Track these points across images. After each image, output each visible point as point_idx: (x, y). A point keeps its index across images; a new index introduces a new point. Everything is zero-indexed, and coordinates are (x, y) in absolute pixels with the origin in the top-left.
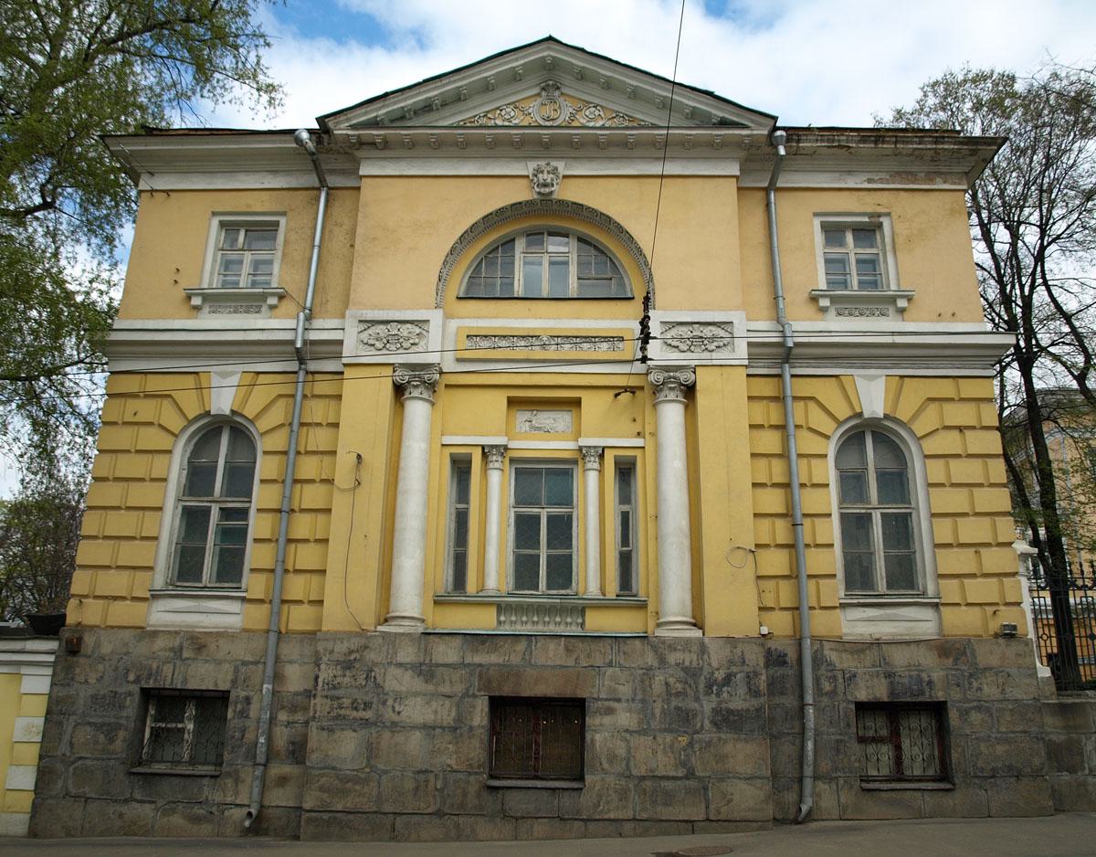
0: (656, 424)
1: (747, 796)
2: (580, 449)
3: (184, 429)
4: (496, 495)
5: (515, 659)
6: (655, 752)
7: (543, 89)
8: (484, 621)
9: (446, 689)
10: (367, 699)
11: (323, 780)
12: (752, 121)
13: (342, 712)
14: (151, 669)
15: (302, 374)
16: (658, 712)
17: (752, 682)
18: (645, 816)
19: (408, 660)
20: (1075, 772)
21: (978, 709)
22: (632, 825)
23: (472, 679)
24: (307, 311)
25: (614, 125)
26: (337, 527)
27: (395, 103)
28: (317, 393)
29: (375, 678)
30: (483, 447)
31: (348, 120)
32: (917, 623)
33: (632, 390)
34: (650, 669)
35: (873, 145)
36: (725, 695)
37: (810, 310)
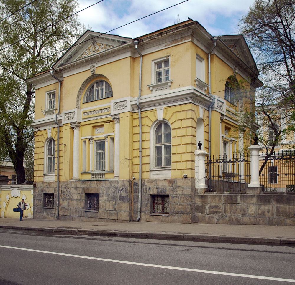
1: (125, 215)
3: (153, 124)
5: (88, 186)
10: (68, 194)
12: (128, 40)
13: (65, 197)
16: (110, 196)
18: (108, 218)
20: (203, 213)
21: (176, 196)
22: (106, 220)
27: (64, 58)
28: (134, 118)
30: (88, 139)
31: (57, 66)
32: (167, 175)
35: (161, 36)
36: (121, 193)
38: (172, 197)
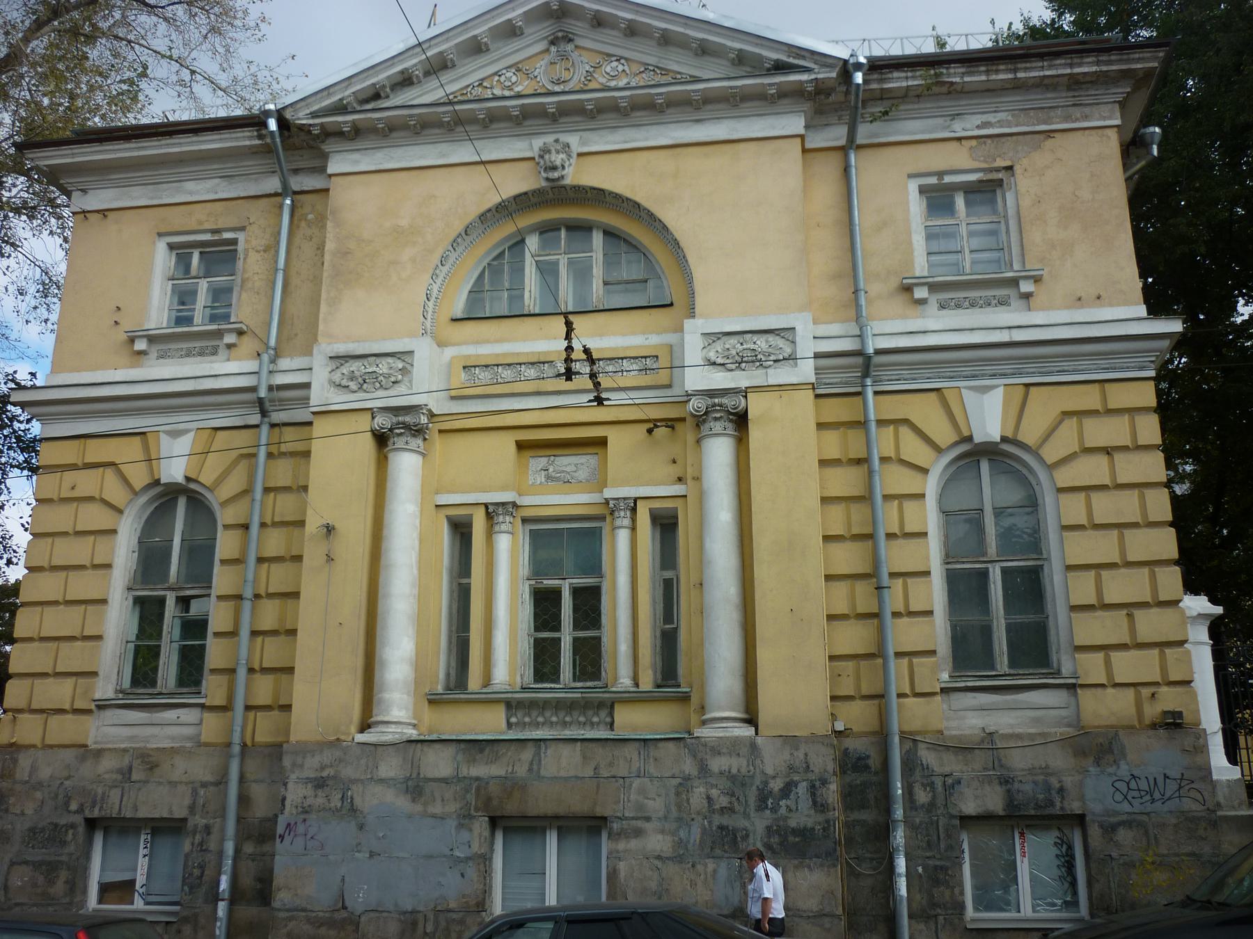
0: (699, 466)
2: (607, 501)
4: (507, 564)
5: (521, 771)
6: (693, 884)
7: (552, 43)
8: (489, 723)
9: (437, 809)
11: (291, 925)
14: (96, 795)
15: (265, 429)
17: (818, 793)
19: (392, 774)
23: (468, 796)
24: (272, 352)
25: (642, 84)
26: (308, 615)
29: (352, 798)
30: (486, 506)
33: (671, 423)
34: (687, 778)
37: (899, 302)
38: (1101, 826)
